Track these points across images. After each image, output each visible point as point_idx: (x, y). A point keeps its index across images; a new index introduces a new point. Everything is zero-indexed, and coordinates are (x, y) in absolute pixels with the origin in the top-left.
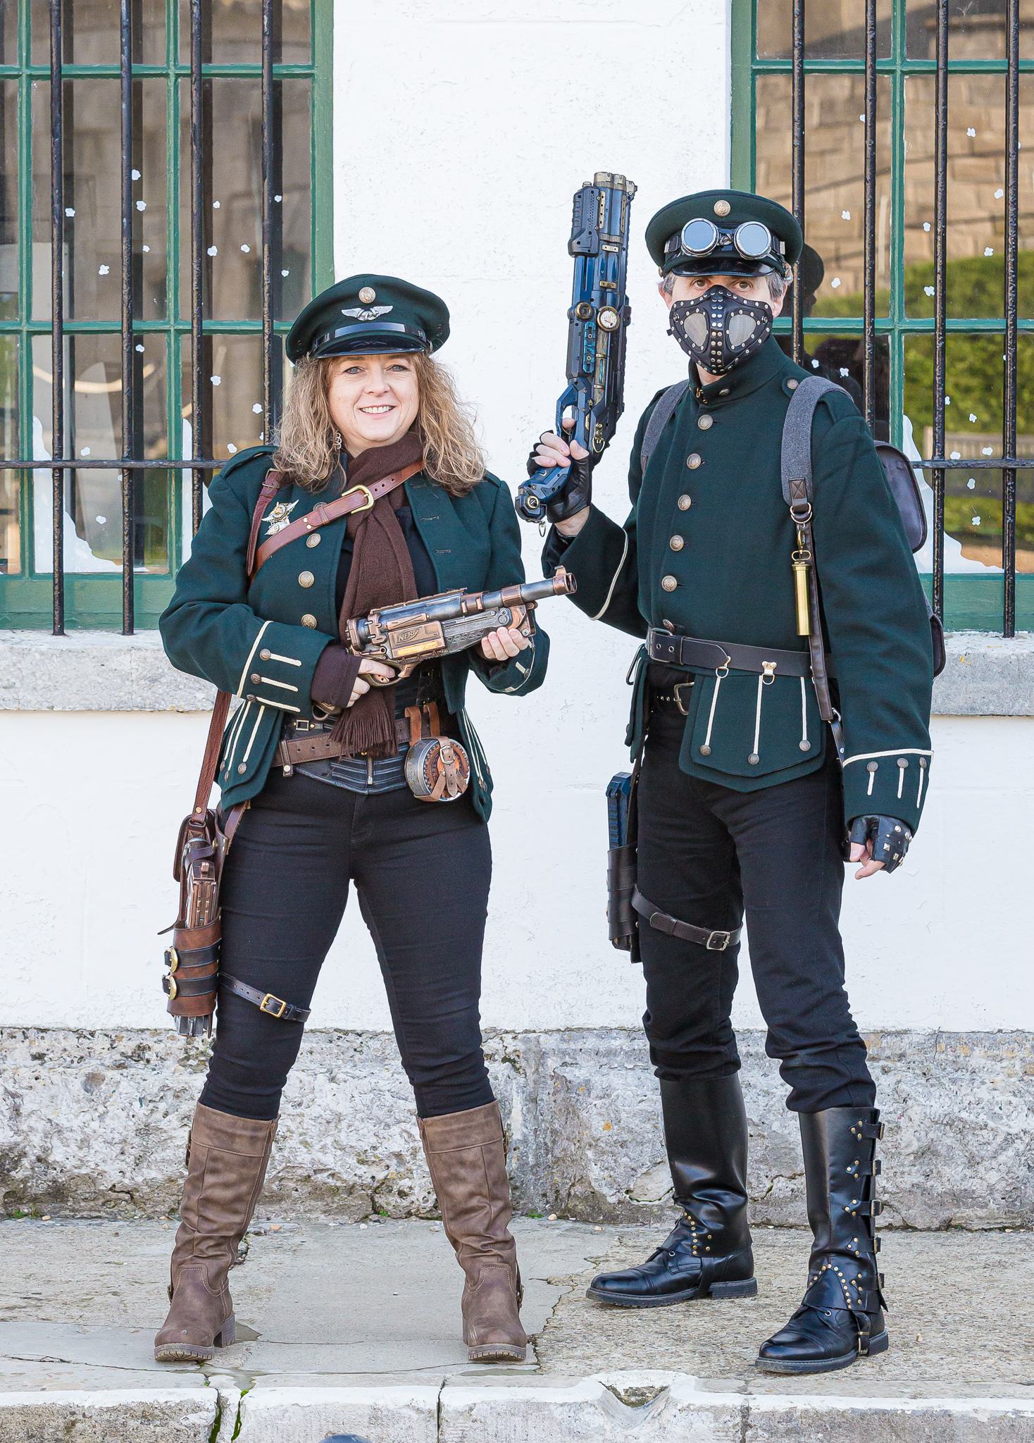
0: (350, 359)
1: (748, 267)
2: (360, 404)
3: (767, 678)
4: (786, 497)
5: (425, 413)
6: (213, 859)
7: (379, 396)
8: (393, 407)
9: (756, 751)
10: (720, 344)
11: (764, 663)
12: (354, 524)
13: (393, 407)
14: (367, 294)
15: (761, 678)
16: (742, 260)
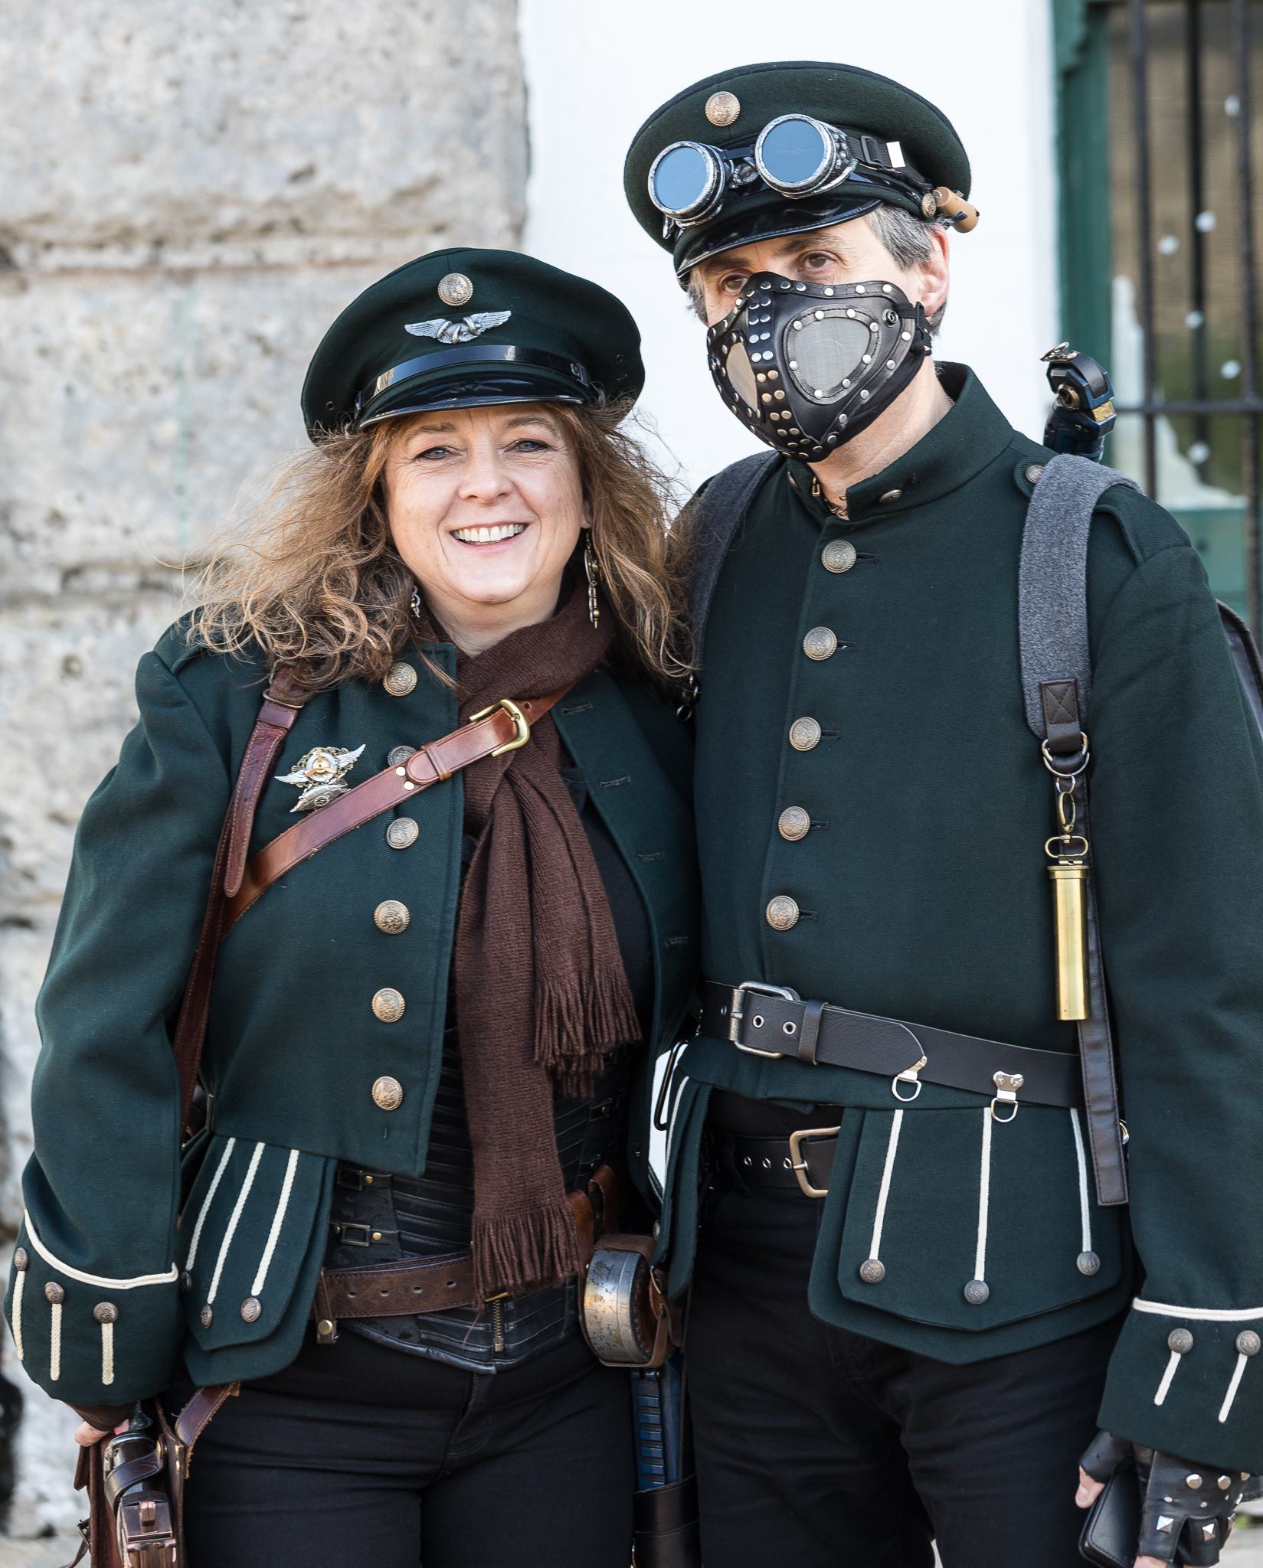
0: (426, 429)
1: (802, 214)
2: (454, 523)
3: (1003, 1108)
4: (1034, 717)
5: (604, 540)
6: (159, 1484)
7: (490, 503)
8: (525, 525)
9: (980, 1274)
10: (779, 394)
11: (999, 1076)
12: (490, 787)
13: (525, 525)
14: (457, 288)
15: (988, 1113)
16: (789, 203)
